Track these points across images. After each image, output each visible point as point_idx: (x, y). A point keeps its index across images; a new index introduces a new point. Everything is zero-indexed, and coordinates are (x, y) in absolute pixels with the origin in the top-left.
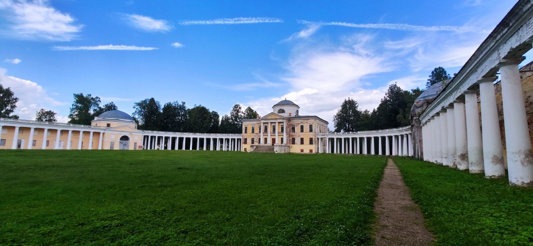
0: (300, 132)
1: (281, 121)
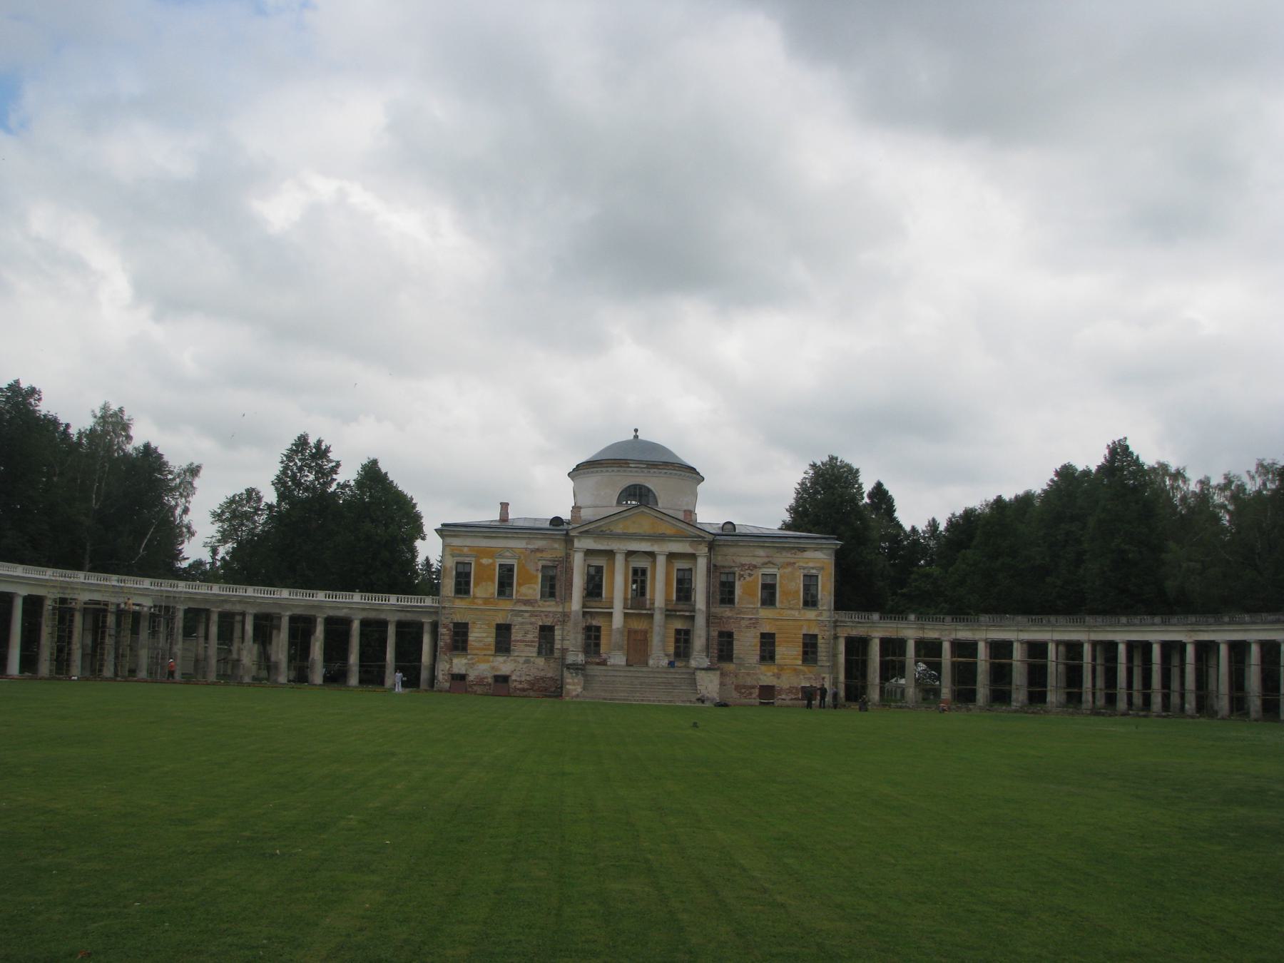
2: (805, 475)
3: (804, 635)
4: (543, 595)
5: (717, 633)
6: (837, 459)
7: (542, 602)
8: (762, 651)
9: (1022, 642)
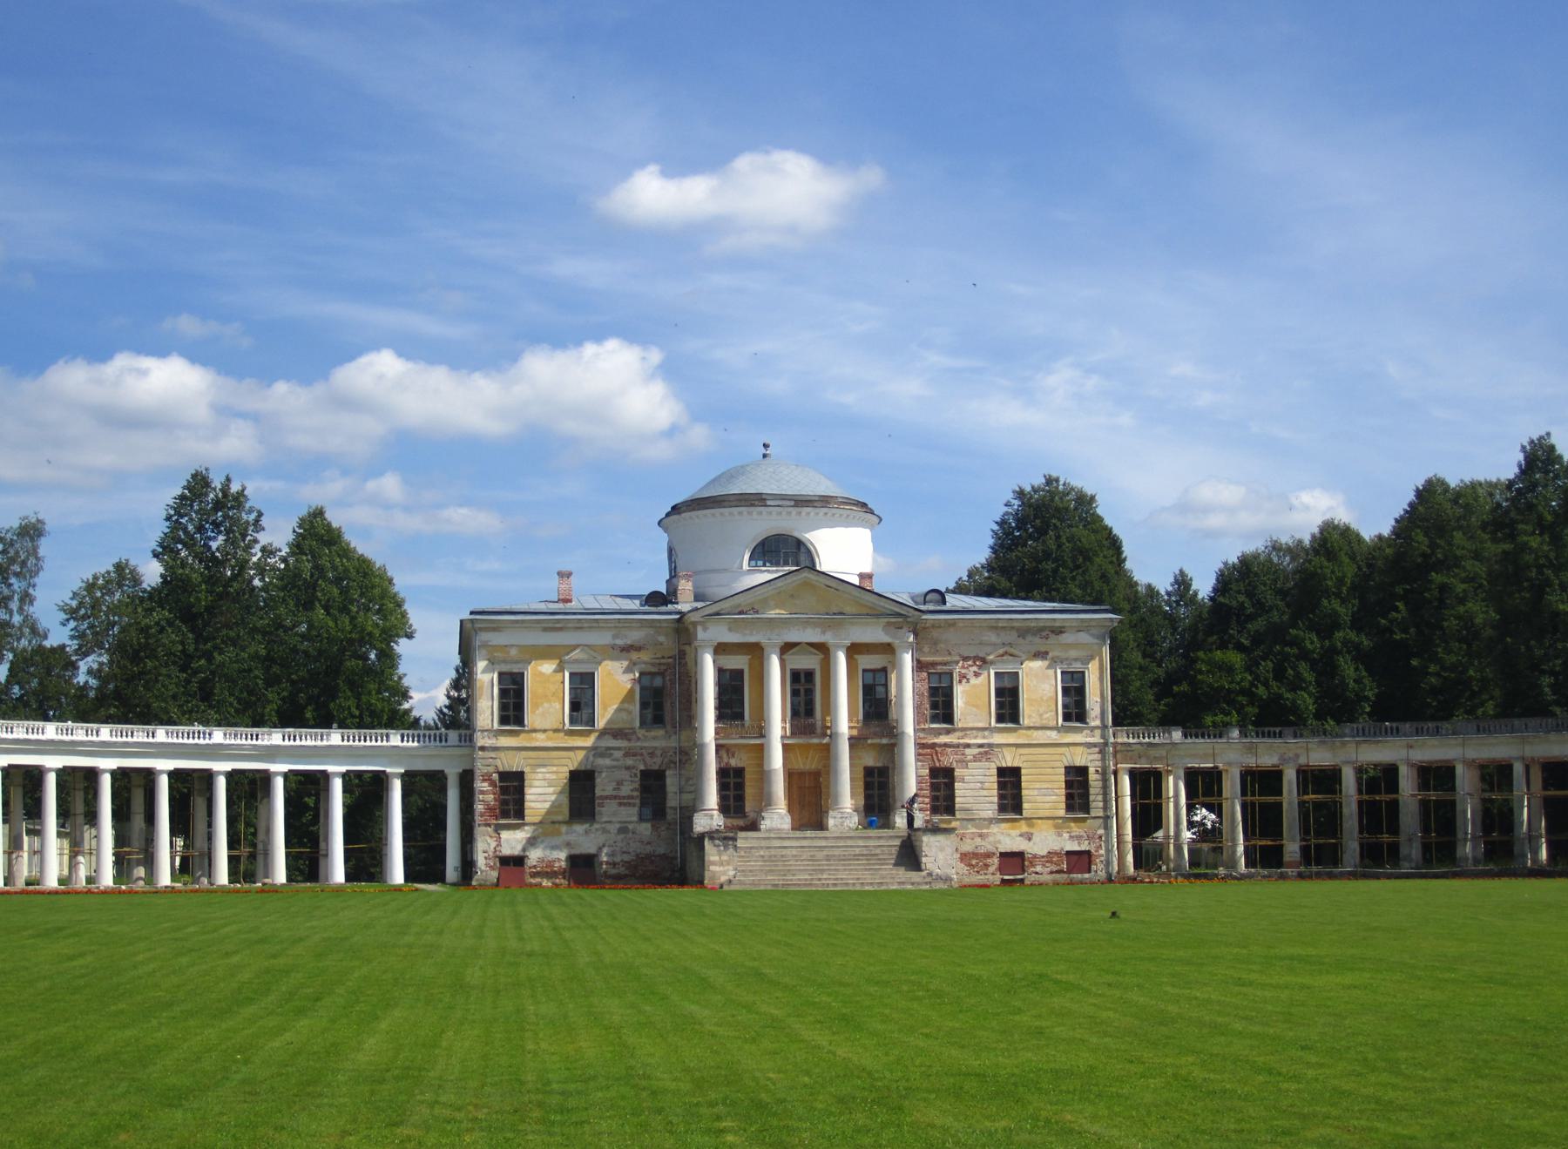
2: (1006, 509)
3: (1066, 768)
4: (643, 723)
5: (928, 771)
6: (1057, 480)
7: (643, 731)
8: (1001, 797)
9: (1469, 763)
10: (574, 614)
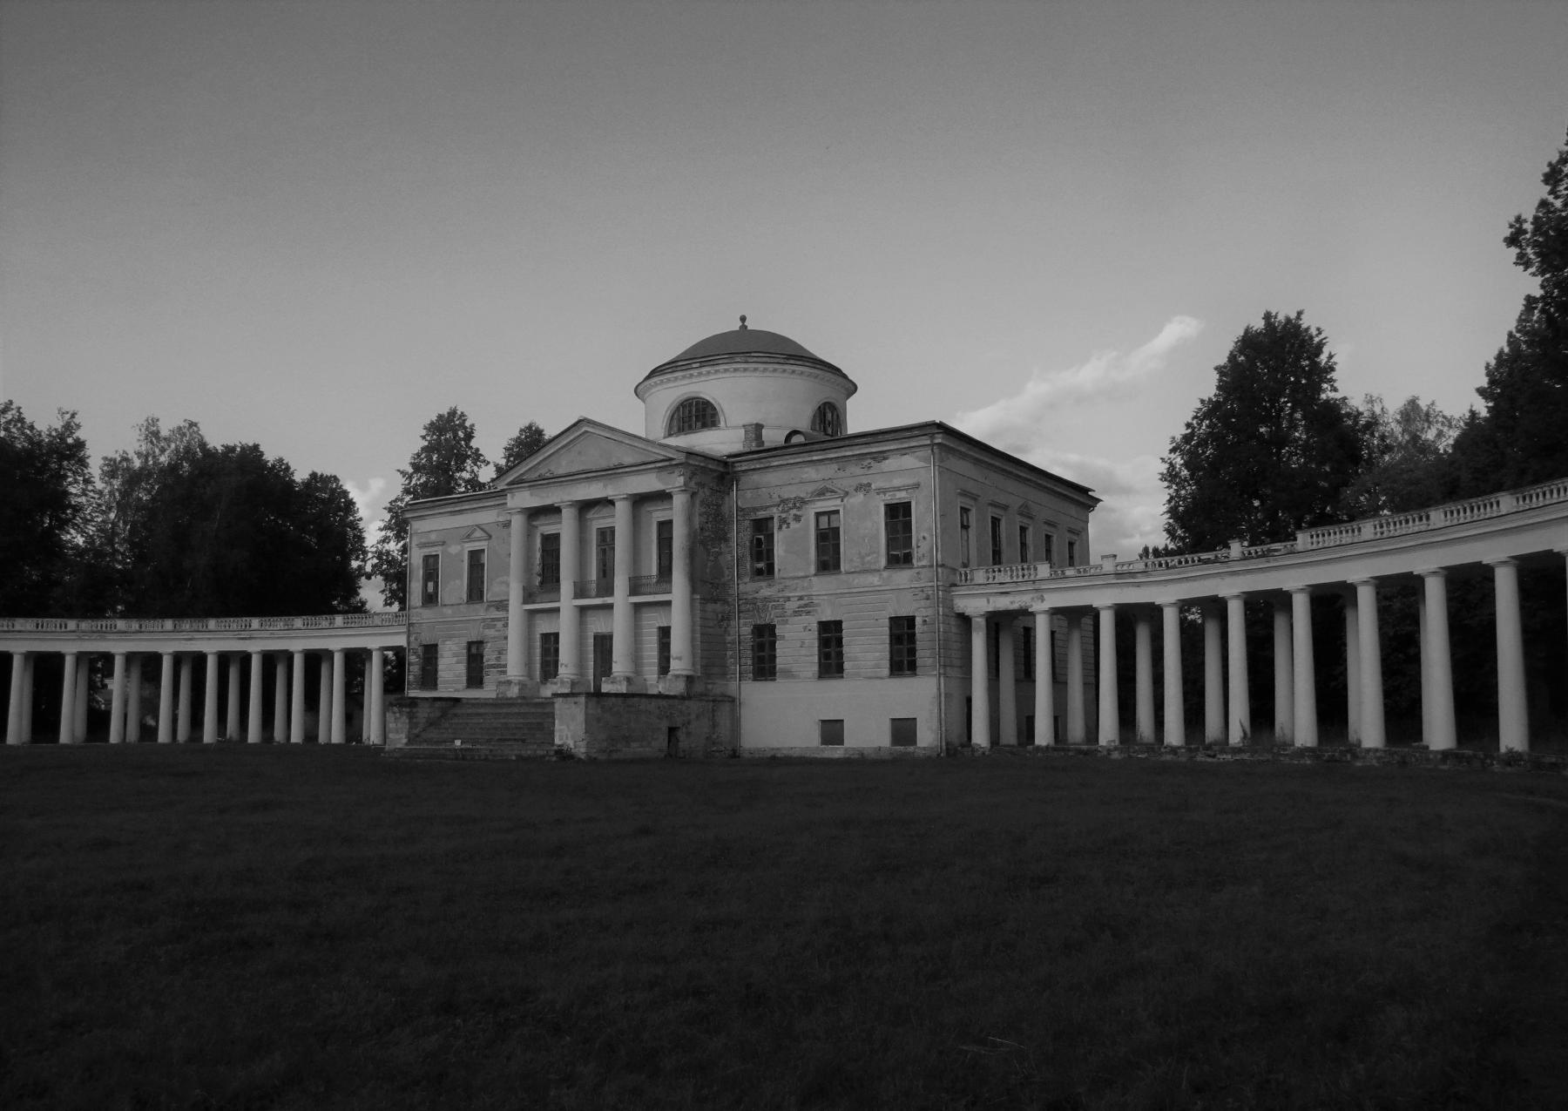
0: (812, 570)
1: (648, 483)
10: (491, 506)
